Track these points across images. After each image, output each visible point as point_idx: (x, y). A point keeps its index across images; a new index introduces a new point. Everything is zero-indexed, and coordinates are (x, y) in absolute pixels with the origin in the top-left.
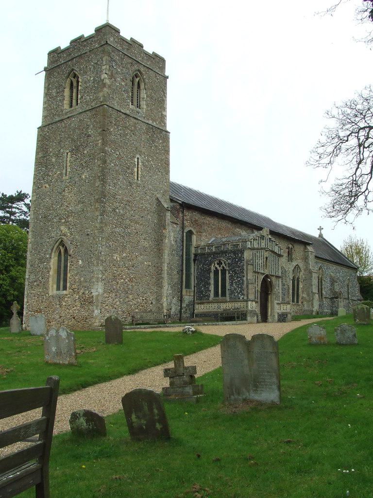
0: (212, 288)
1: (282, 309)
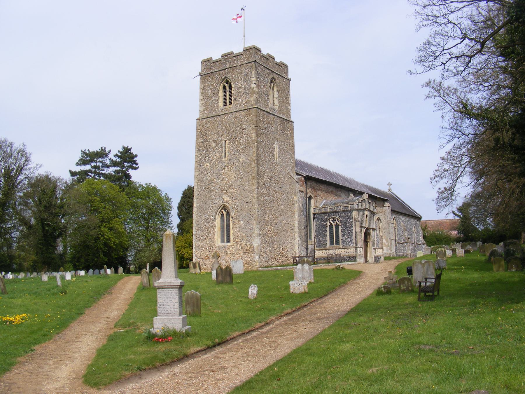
0: (328, 238)
1: (377, 253)
